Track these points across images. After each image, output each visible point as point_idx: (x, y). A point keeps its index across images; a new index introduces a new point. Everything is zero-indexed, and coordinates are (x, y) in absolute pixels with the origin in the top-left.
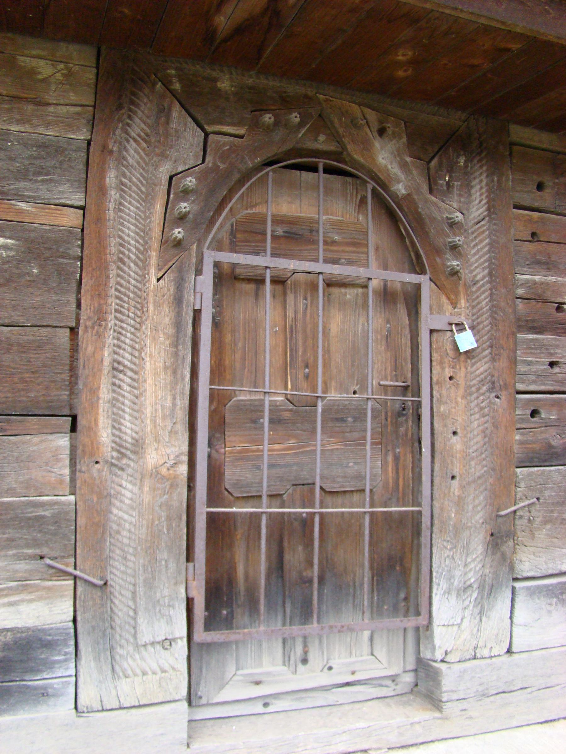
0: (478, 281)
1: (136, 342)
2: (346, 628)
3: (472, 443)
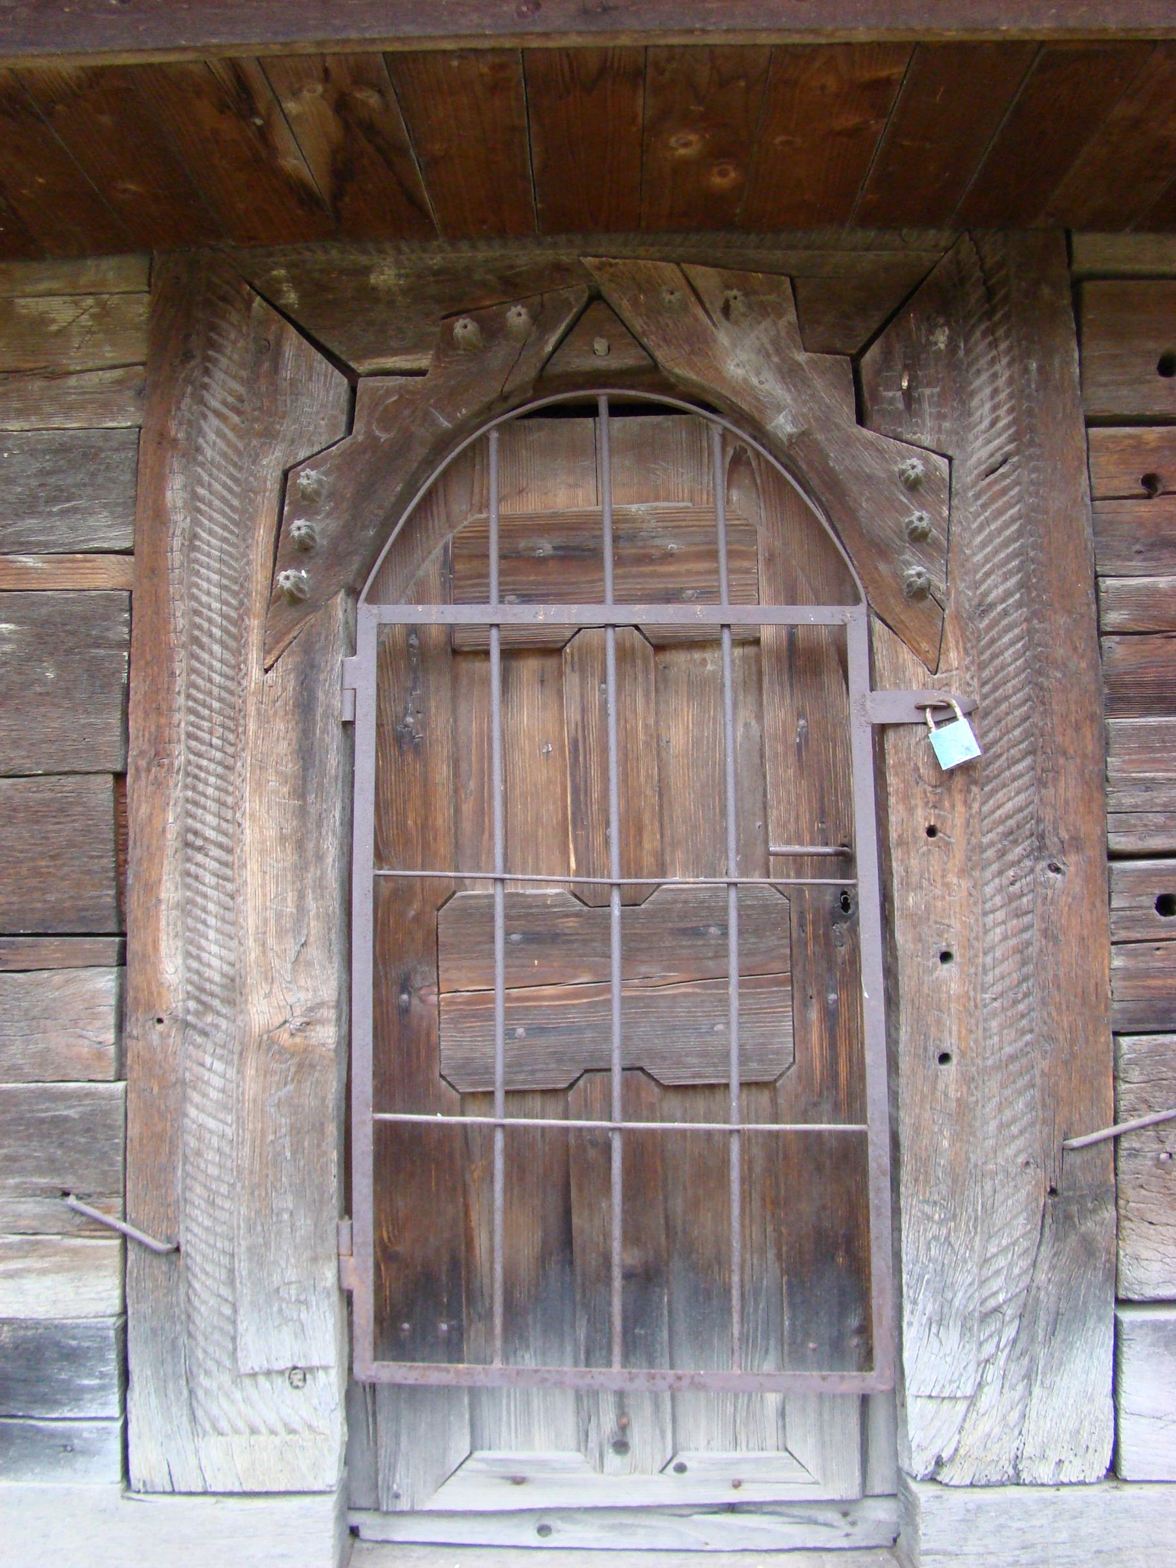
0: (992, 606)
1: (226, 792)
2: (685, 1382)
3: (989, 978)
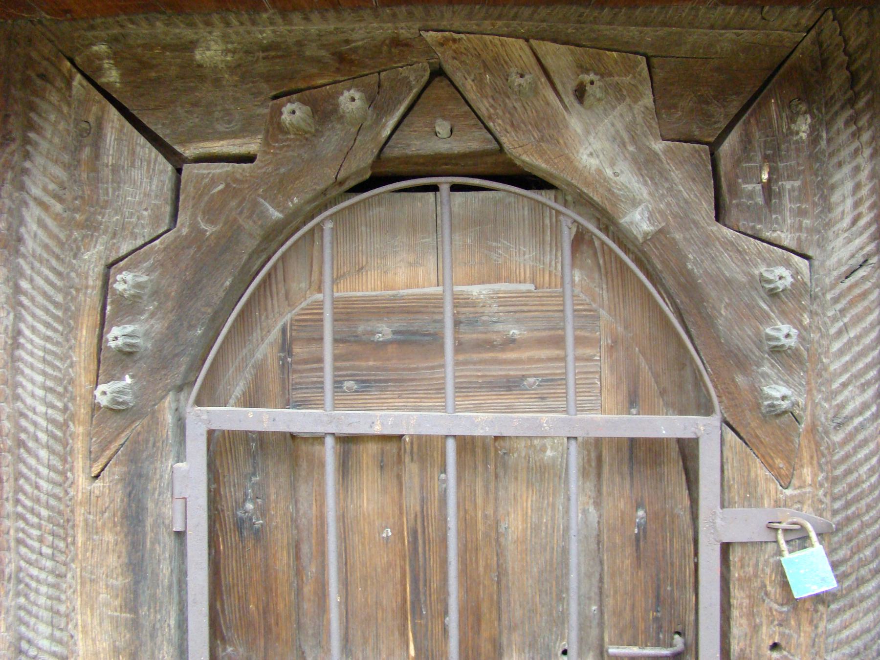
0: (850, 418)
